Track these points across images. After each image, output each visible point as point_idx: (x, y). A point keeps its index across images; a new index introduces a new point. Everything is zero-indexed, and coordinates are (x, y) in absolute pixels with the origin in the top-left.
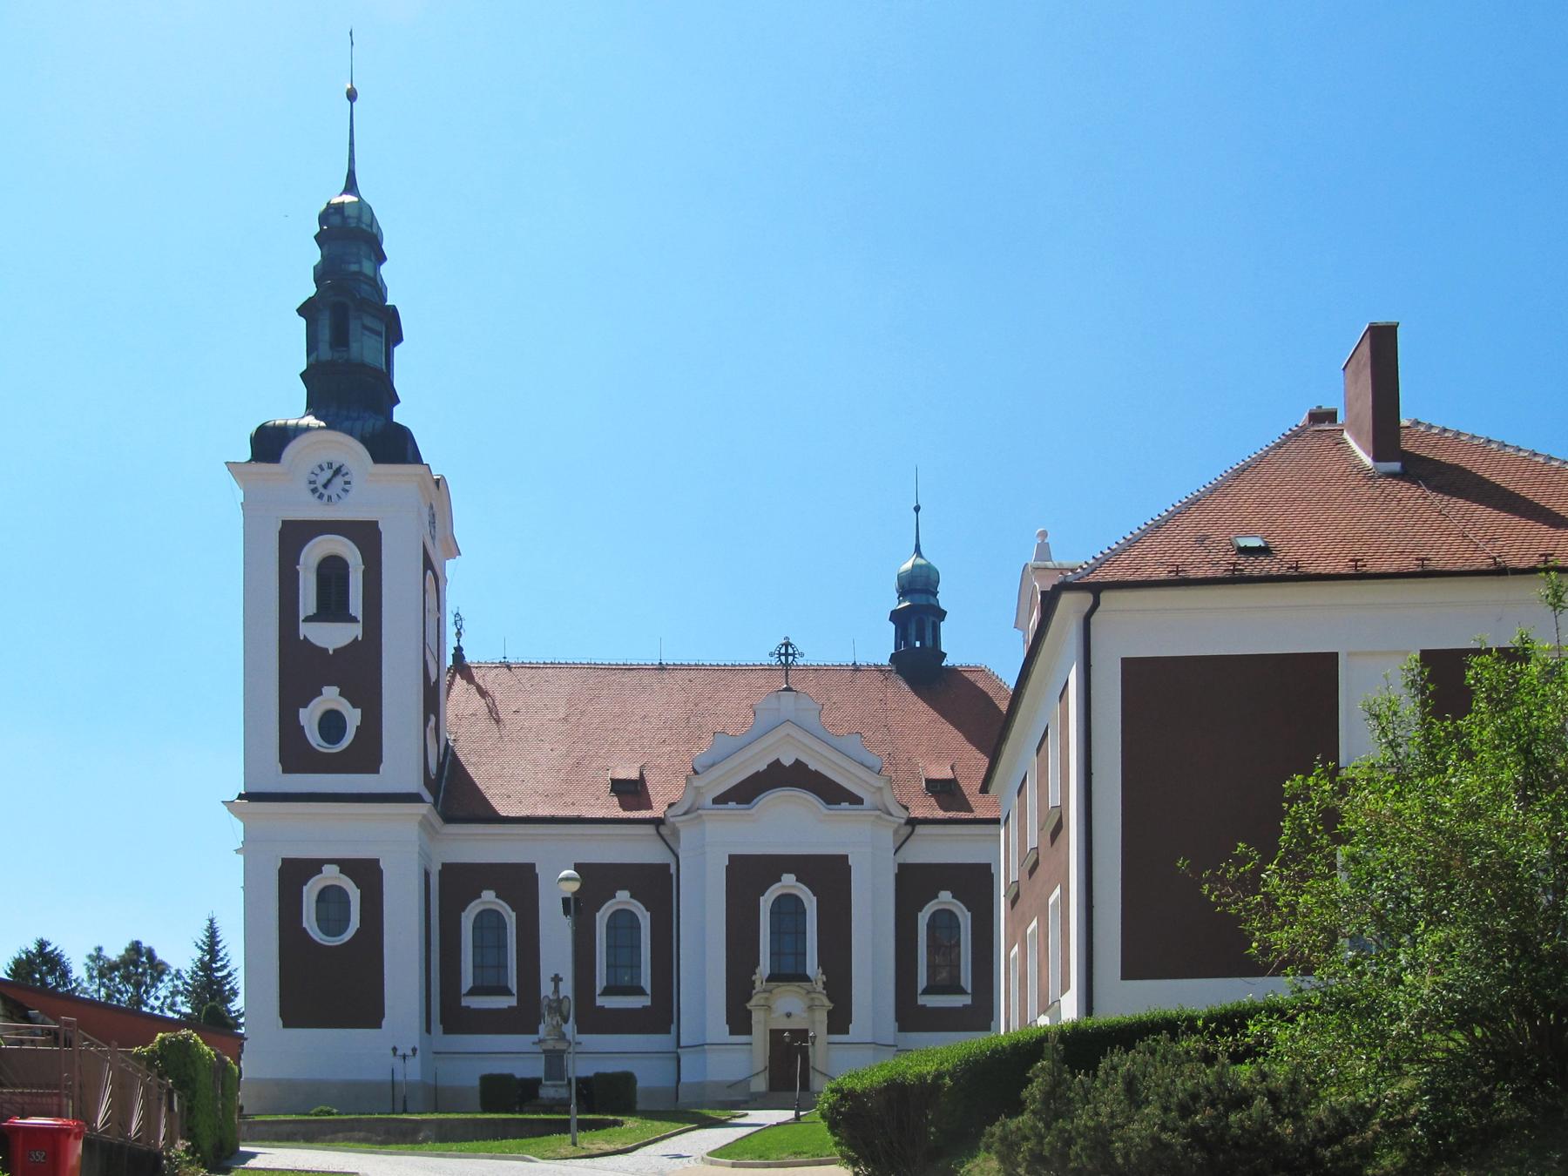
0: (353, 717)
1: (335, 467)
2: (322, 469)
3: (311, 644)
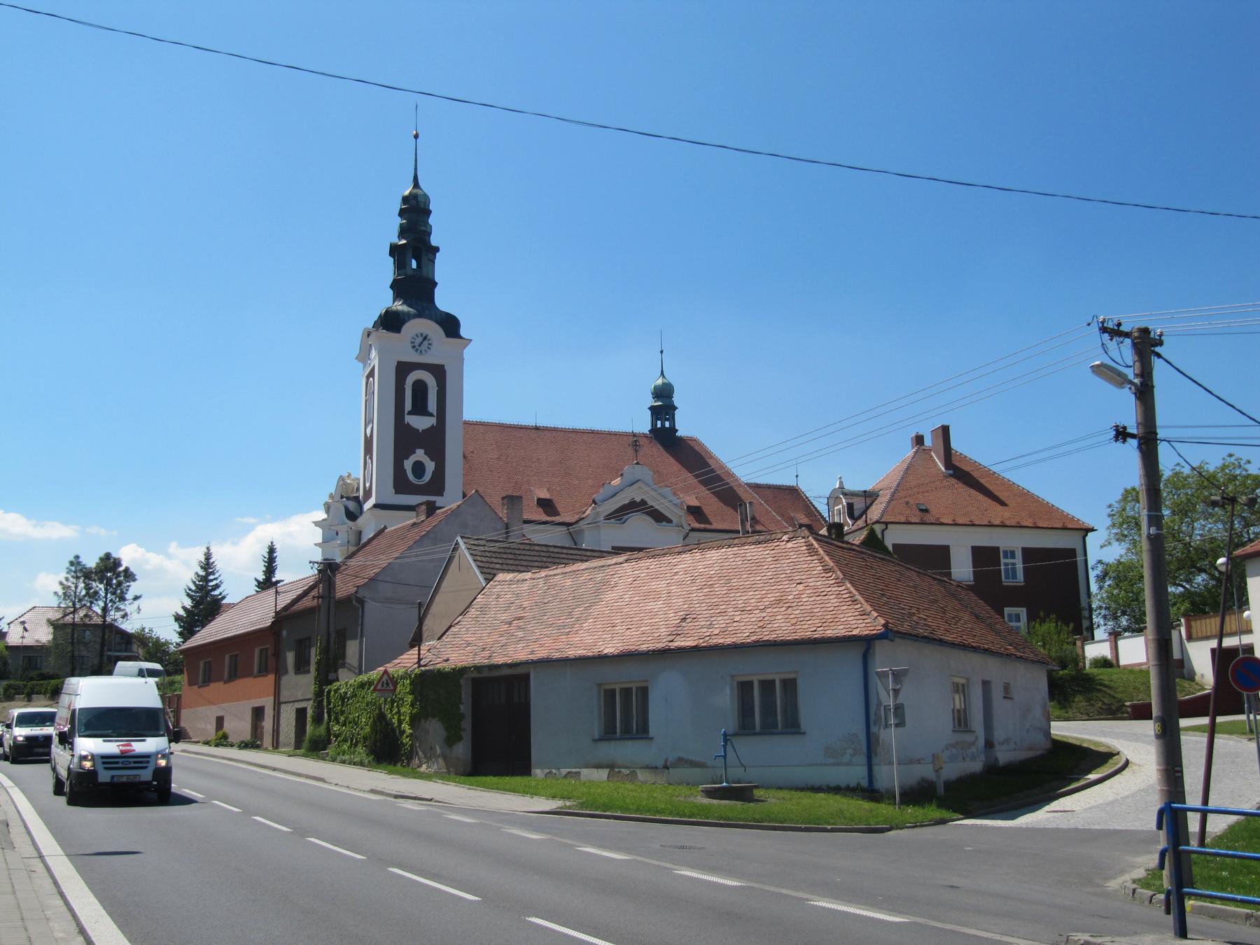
0: (430, 466)
1: (424, 335)
2: (418, 337)
3: (411, 426)
